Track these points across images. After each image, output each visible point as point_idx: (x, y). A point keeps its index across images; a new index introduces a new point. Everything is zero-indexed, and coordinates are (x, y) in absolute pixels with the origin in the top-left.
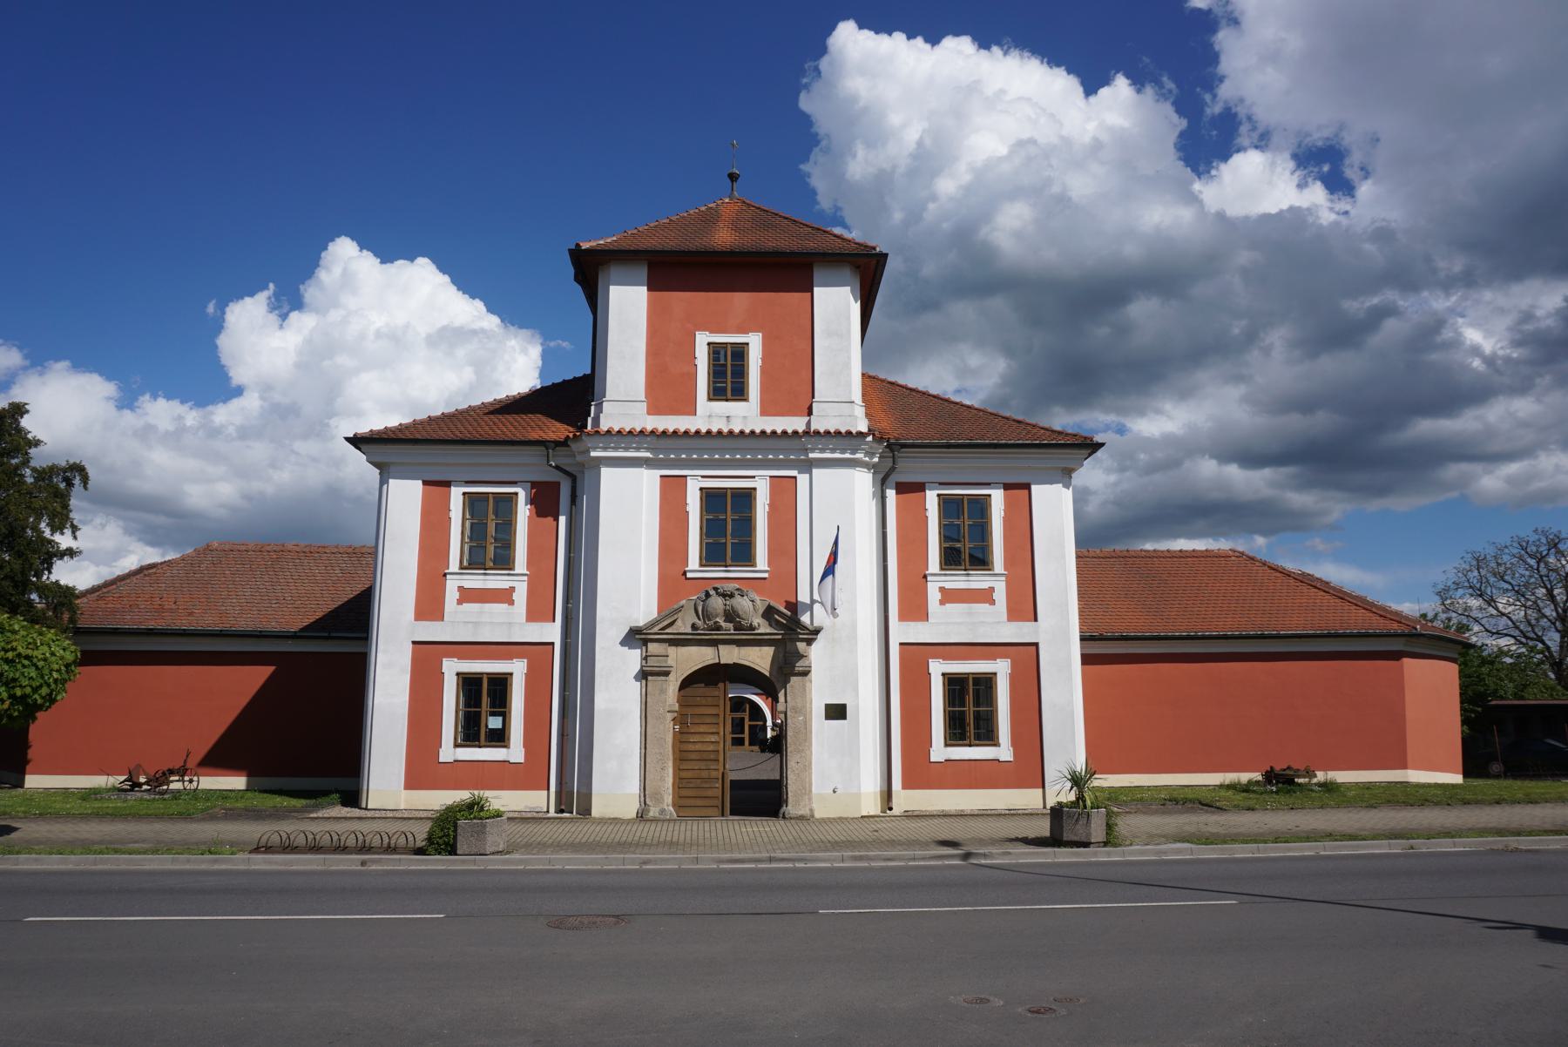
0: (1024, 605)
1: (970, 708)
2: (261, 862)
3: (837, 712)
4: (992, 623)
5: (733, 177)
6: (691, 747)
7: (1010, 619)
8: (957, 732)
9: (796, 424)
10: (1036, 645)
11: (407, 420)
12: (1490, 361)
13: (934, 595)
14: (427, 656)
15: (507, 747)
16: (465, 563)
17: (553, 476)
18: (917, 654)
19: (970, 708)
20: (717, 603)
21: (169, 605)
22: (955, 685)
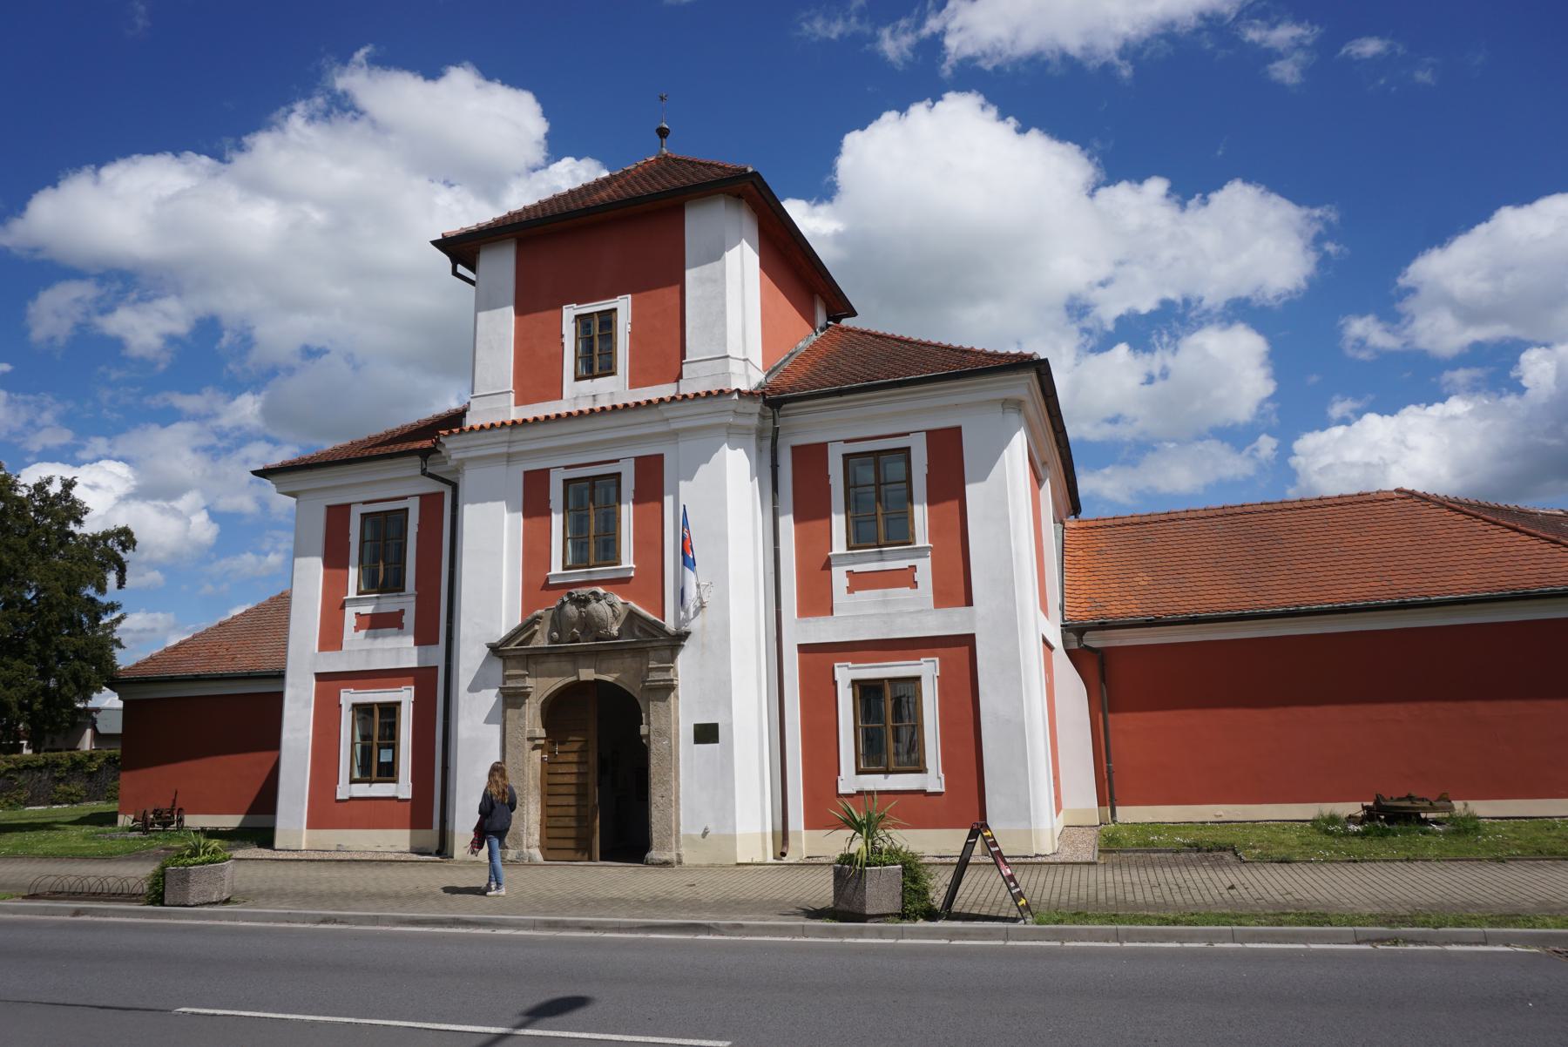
0: (956, 586)
1: (886, 720)
2: (1207, 883)
3: (706, 734)
4: (914, 612)
5: (663, 133)
6: (559, 779)
7: (936, 606)
8: (873, 756)
9: (666, 390)
10: (972, 636)
11: (347, 442)
12: (1251, 25)
15: (395, 781)
16: (1094, 640)
17: (431, 487)
19: (886, 720)
20: (571, 610)
21: (222, 652)
22: (867, 691)
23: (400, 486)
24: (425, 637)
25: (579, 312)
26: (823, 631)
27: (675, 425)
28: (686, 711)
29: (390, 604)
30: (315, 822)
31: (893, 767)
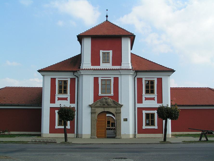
3: (126, 120)
13: (144, 99)
14: (52, 110)
17: (73, 77)
18: (140, 110)
23: (67, 77)
24: (72, 101)
25: (103, 52)
26: (53, 105)
27: (121, 73)
28: (123, 117)
29: (151, 96)
30: (51, 132)
31: (150, 125)
